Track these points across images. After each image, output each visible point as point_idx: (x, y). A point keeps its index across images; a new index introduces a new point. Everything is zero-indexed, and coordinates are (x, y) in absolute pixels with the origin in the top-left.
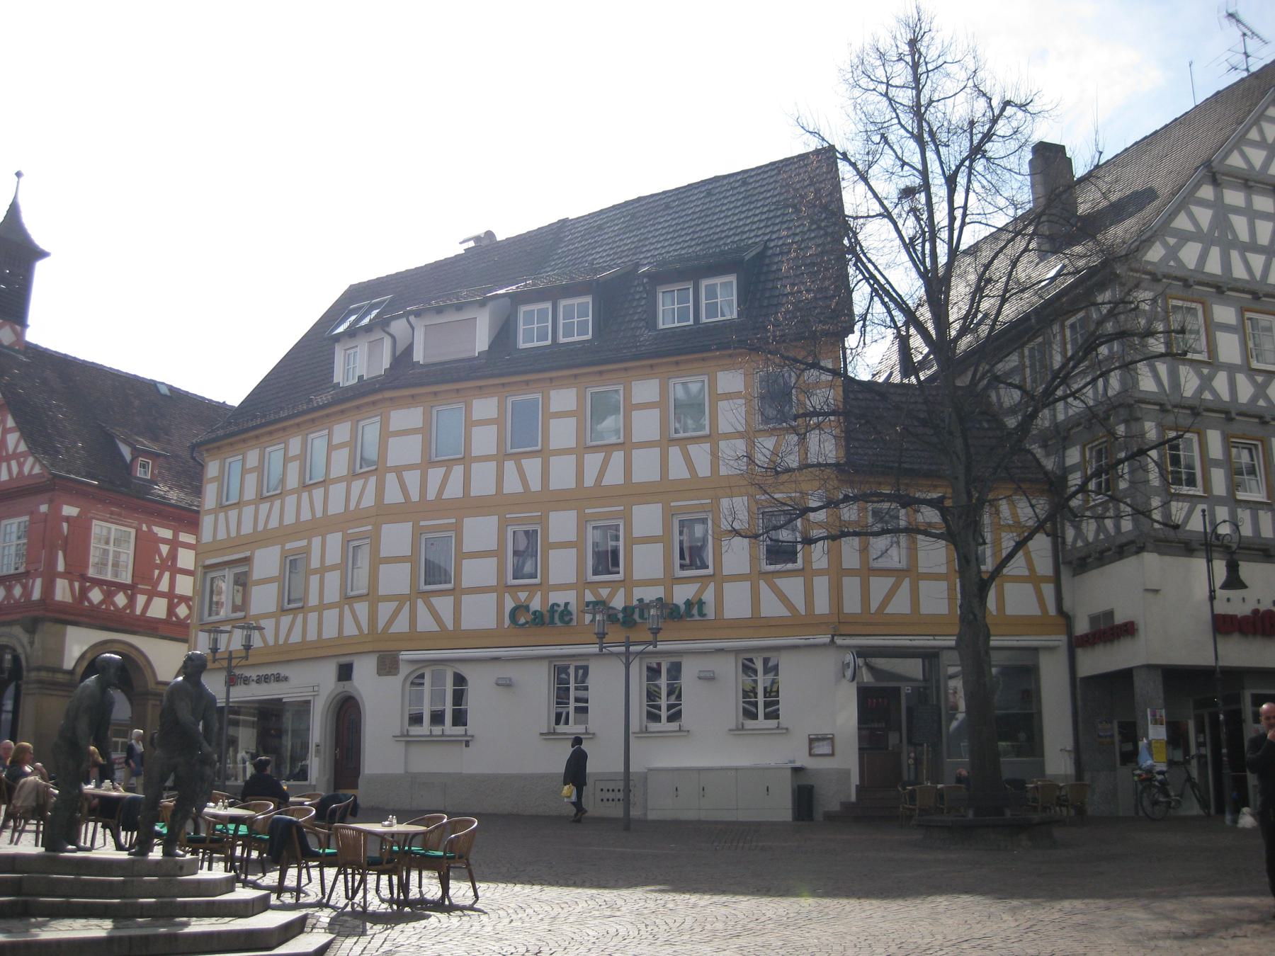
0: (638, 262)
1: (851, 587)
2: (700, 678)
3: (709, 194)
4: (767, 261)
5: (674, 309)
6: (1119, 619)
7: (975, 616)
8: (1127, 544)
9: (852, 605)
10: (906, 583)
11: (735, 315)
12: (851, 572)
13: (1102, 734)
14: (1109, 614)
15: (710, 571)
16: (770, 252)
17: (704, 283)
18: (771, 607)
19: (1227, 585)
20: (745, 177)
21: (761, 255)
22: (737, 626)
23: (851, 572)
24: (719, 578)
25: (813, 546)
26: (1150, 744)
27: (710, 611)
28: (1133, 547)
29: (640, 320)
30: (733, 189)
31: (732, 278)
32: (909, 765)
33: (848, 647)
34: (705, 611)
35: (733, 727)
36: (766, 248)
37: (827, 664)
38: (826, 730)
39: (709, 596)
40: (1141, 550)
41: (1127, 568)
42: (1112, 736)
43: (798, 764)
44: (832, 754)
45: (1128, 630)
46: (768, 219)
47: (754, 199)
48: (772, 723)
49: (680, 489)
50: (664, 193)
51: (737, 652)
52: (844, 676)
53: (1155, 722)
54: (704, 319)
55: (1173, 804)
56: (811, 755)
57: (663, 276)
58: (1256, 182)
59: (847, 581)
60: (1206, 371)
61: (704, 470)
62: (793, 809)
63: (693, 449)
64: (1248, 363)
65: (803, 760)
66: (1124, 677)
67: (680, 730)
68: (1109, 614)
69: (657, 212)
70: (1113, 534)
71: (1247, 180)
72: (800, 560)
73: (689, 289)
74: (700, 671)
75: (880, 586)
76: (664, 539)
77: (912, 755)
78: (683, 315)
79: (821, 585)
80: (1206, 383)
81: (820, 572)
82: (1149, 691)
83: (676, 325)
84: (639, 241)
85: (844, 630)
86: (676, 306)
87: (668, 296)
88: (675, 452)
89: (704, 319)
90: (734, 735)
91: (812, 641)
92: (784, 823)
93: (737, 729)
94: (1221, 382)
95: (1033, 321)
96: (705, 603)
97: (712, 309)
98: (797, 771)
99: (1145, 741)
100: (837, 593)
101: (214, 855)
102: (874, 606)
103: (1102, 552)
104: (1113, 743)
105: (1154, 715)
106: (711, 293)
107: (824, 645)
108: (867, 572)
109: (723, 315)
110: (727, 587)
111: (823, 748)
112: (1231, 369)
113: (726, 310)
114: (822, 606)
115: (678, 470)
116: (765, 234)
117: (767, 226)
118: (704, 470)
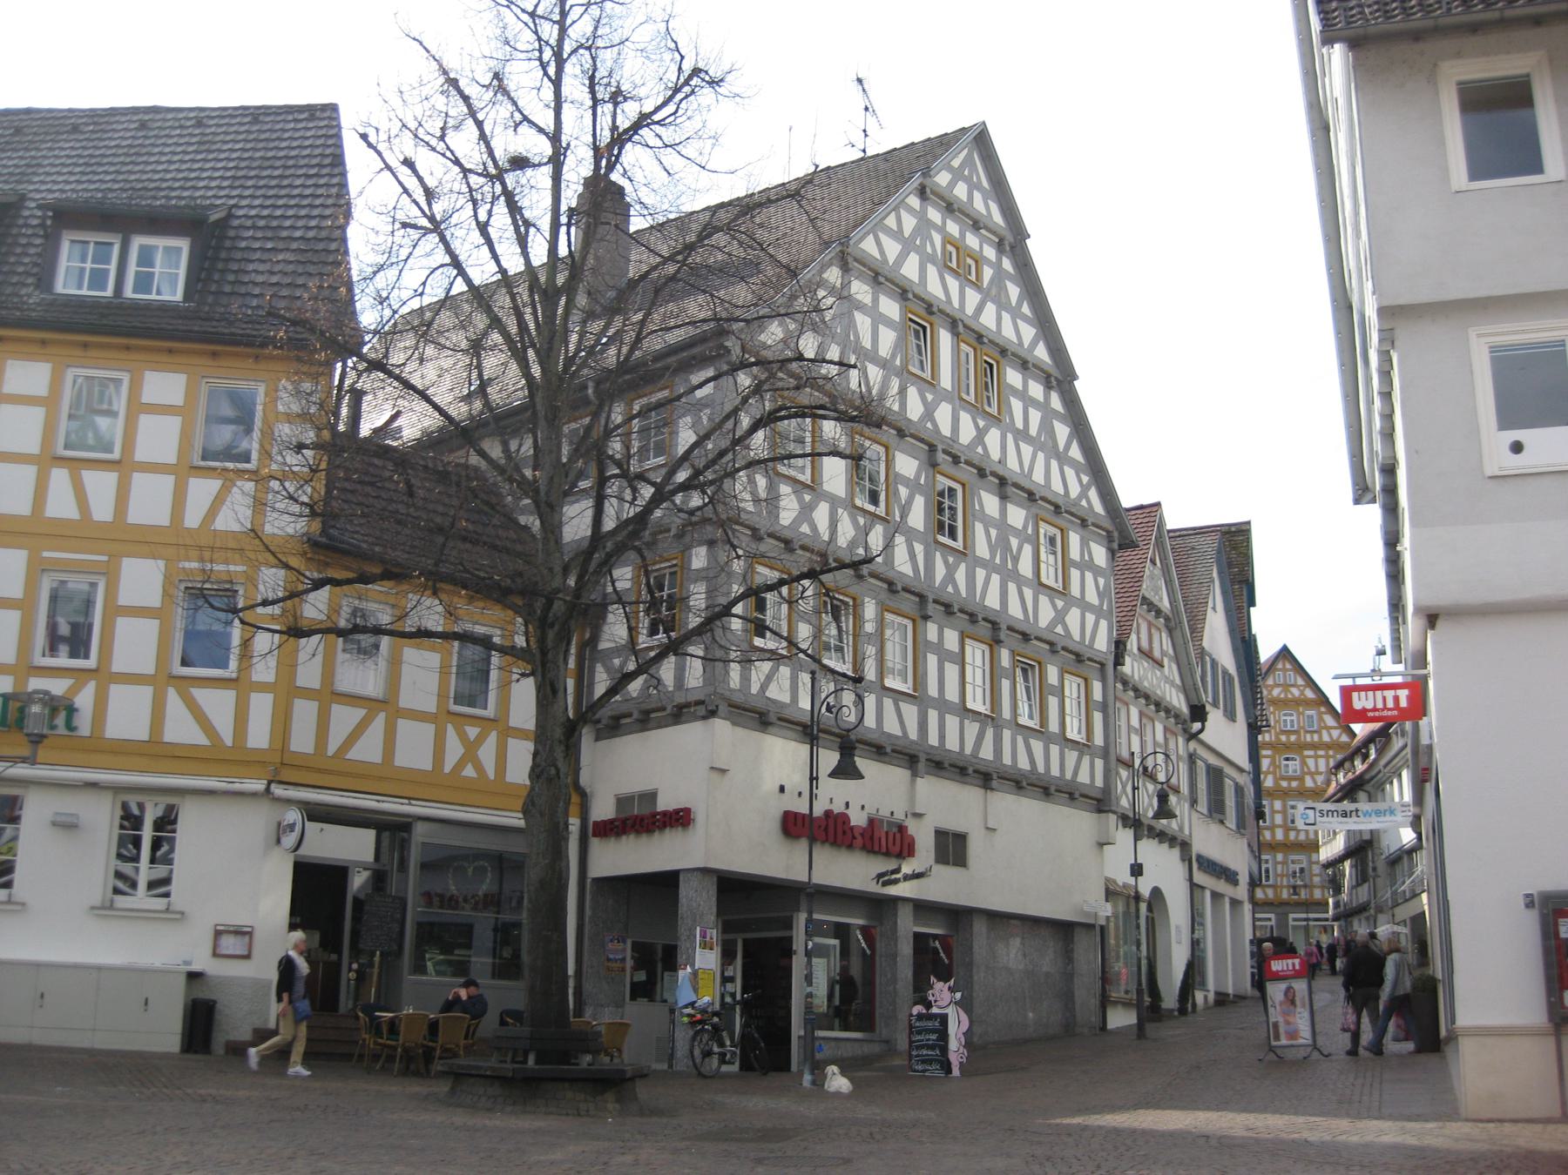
0: (24, 195)
1: (305, 713)
2: (54, 824)
3: (143, 126)
4: (232, 233)
5: (82, 270)
6: (665, 803)
7: (558, 770)
8: (688, 705)
9: (302, 741)
10: (380, 721)
11: (178, 296)
12: (307, 693)
13: (611, 956)
14: (651, 796)
15: (91, 663)
16: (236, 223)
17: (138, 241)
18: (181, 729)
19: (836, 773)
20: (200, 118)
21: (223, 223)
22: (124, 751)
23: (307, 693)
24: (104, 676)
25: (303, 641)
26: (695, 974)
27: (84, 725)
28: (701, 710)
29: (28, 274)
30: (181, 127)
31: (183, 245)
32: (349, 980)
33: (289, 802)
34: (76, 722)
35: (98, 903)
36: (230, 216)
37: (255, 822)
38: (241, 919)
39: (85, 700)
40: (712, 713)
41: (689, 735)
42: (623, 960)
43: (195, 967)
44: (248, 957)
45: (680, 819)
46: (234, 178)
47: (214, 147)
48: (160, 903)
49: (62, 533)
50: (70, 110)
51: (117, 789)
52: (278, 841)
53: (704, 945)
54: (128, 292)
55: (728, 1056)
56: (215, 954)
57: (68, 216)
58: (887, 279)
59: (299, 704)
60: (807, 498)
61: (102, 511)
62: (183, 1034)
63: (90, 477)
64: (852, 499)
65: (202, 961)
66: (667, 882)
67: (9, 902)
68: (651, 796)
69: (58, 133)
70: (671, 689)
71: (877, 274)
72: (233, 664)
73: (111, 244)
74: (57, 814)
75: (344, 718)
76: (24, 605)
77: (355, 966)
78: (98, 279)
79: (262, 707)
80: (806, 511)
81: (263, 687)
82: (698, 902)
83: (85, 292)
84: (28, 166)
85: (287, 775)
86: (88, 265)
87: (78, 247)
88: (60, 478)
89: (128, 292)
90: (98, 915)
91: (237, 787)
92: (166, 1056)
93: (103, 908)
94: (821, 514)
95: (590, 391)
96: (76, 710)
97: (144, 282)
98: (194, 977)
99: (689, 969)
100: (282, 722)
101: (820, 1033)
102: (332, 749)
103: (647, 713)
104: (623, 970)
105: (703, 935)
106: (146, 258)
107: (254, 795)
108: (329, 695)
109: (158, 293)
110: (116, 691)
111: (230, 944)
112: (834, 501)
113: (165, 288)
114: (259, 736)
115: (61, 504)
116: (228, 197)
117: (232, 187)
118: (102, 511)
